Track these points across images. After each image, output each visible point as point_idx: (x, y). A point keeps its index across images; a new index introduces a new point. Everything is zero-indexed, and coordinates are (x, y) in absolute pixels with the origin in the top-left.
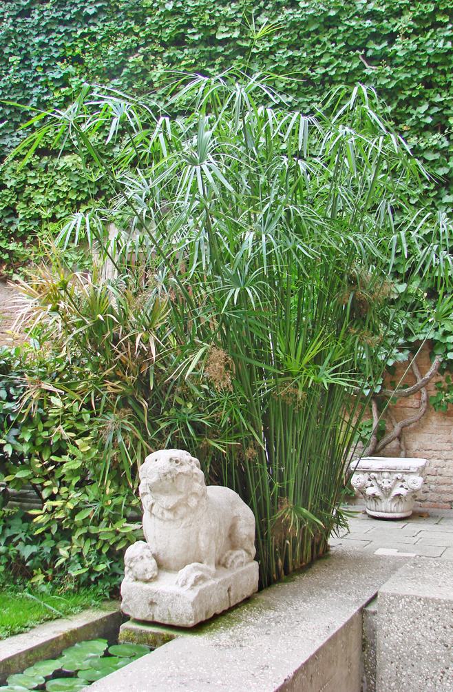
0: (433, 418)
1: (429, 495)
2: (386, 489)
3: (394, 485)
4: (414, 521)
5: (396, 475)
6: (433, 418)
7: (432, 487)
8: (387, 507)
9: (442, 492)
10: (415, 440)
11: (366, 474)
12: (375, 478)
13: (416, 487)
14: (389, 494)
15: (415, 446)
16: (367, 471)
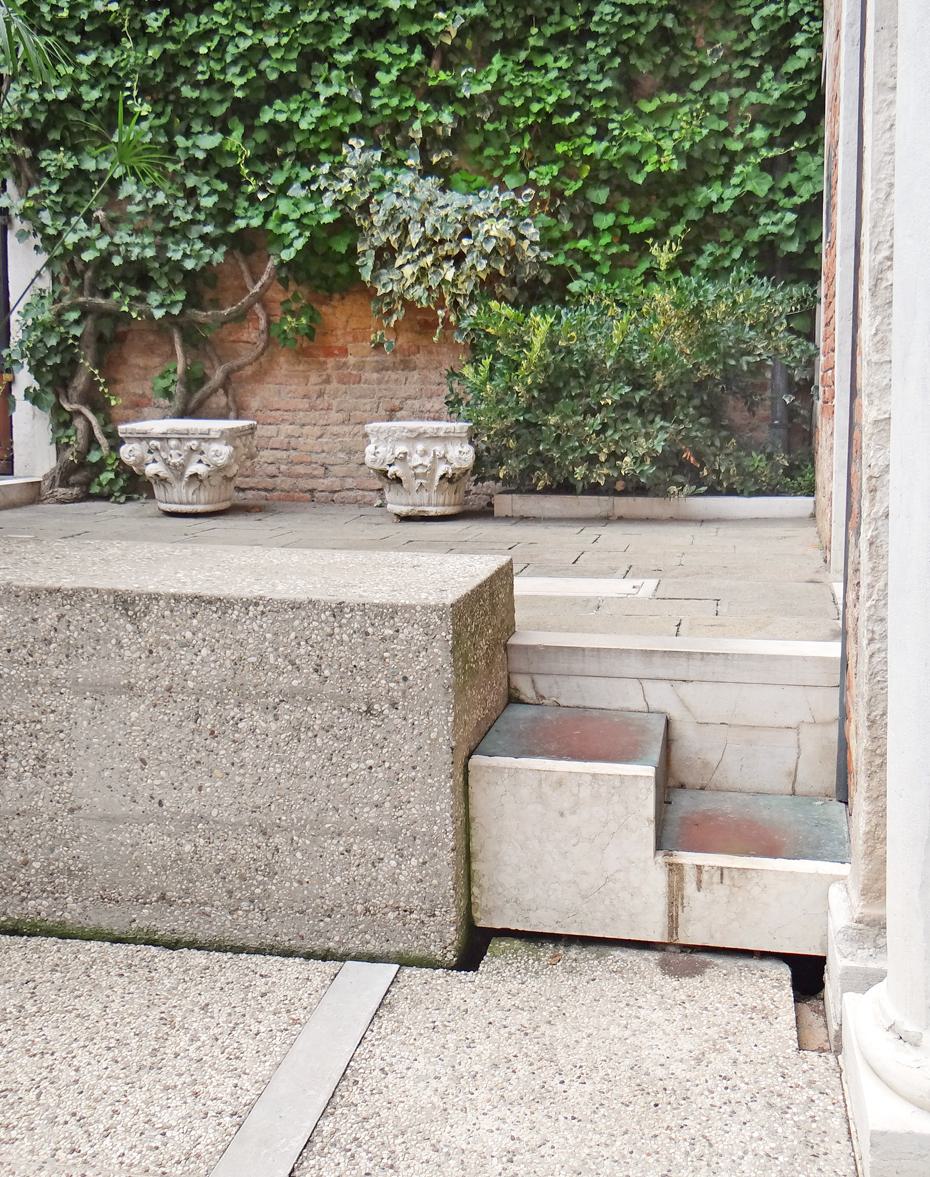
0: (282, 359)
1: (278, 480)
2: (174, 464)
3: (188, 459)
4: (230, 517)
5: (190, 444)
6: (282, 359)
7: (283, 467)
8: (179, 495)
9: (298, 476)
10: (254, 394)
11: (144, 443)
12: (157, 449)
13: (221, 461)
14: (182, 474)
15: (254, 404)
16: (144, 438)
